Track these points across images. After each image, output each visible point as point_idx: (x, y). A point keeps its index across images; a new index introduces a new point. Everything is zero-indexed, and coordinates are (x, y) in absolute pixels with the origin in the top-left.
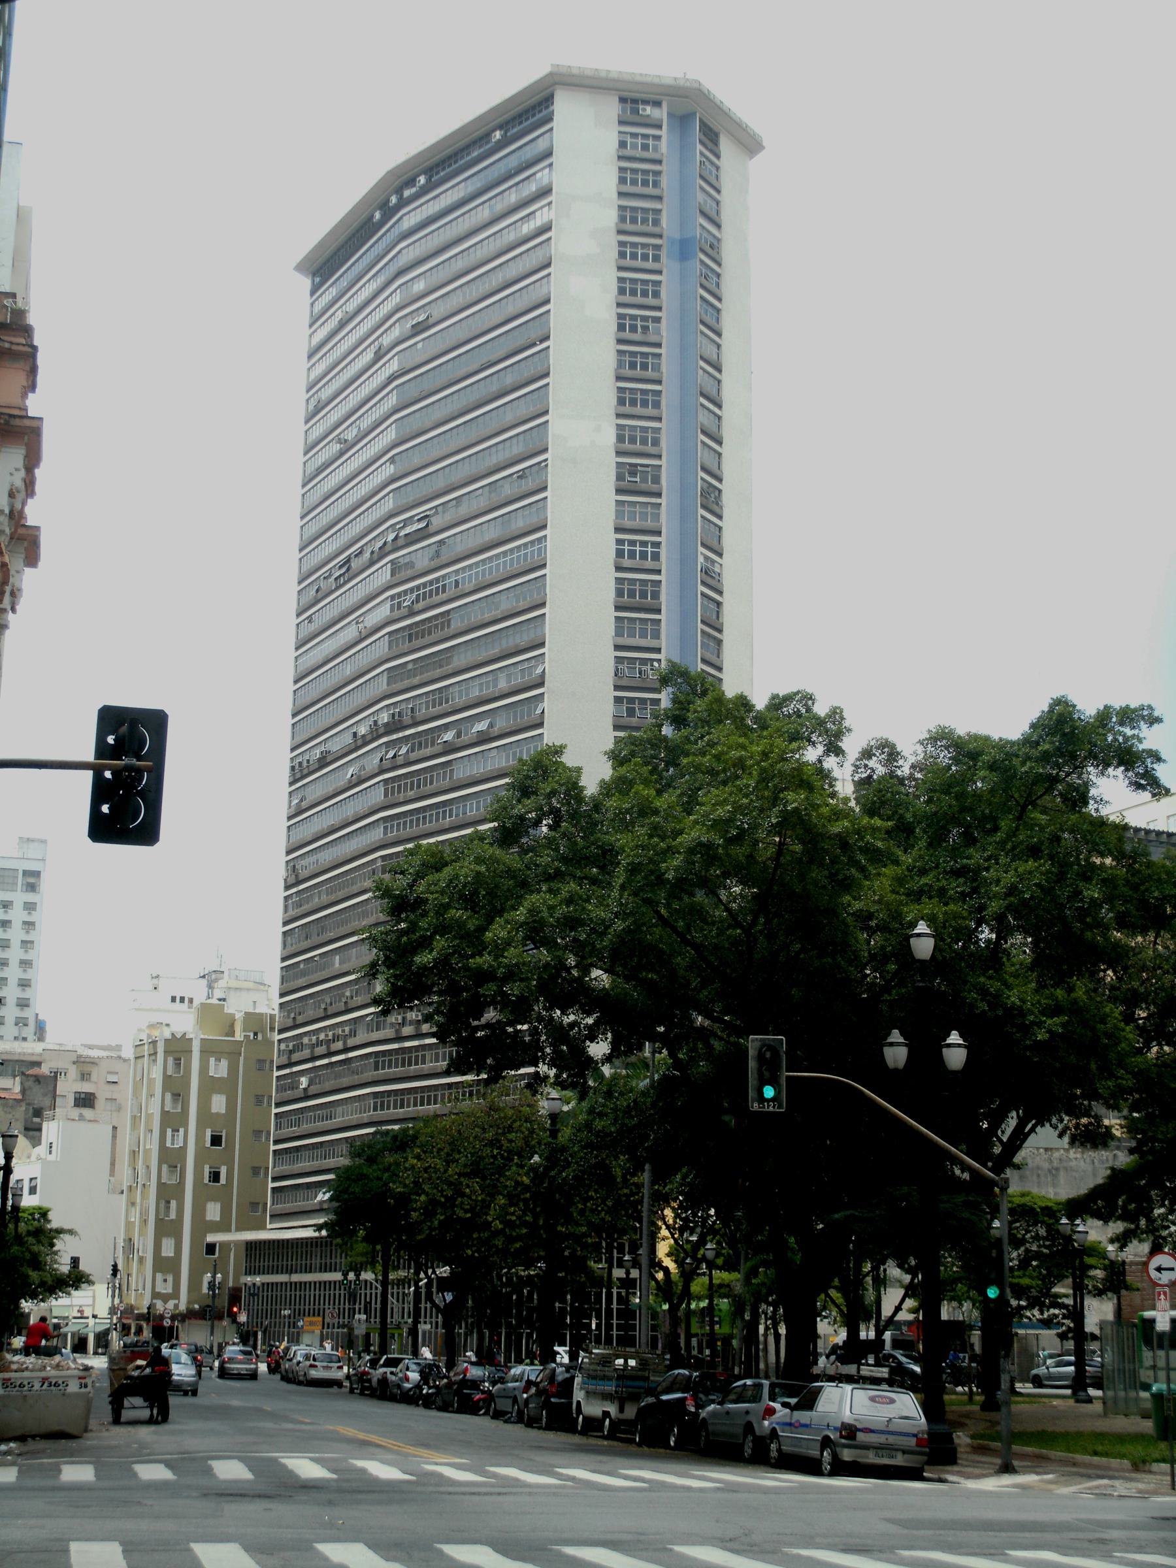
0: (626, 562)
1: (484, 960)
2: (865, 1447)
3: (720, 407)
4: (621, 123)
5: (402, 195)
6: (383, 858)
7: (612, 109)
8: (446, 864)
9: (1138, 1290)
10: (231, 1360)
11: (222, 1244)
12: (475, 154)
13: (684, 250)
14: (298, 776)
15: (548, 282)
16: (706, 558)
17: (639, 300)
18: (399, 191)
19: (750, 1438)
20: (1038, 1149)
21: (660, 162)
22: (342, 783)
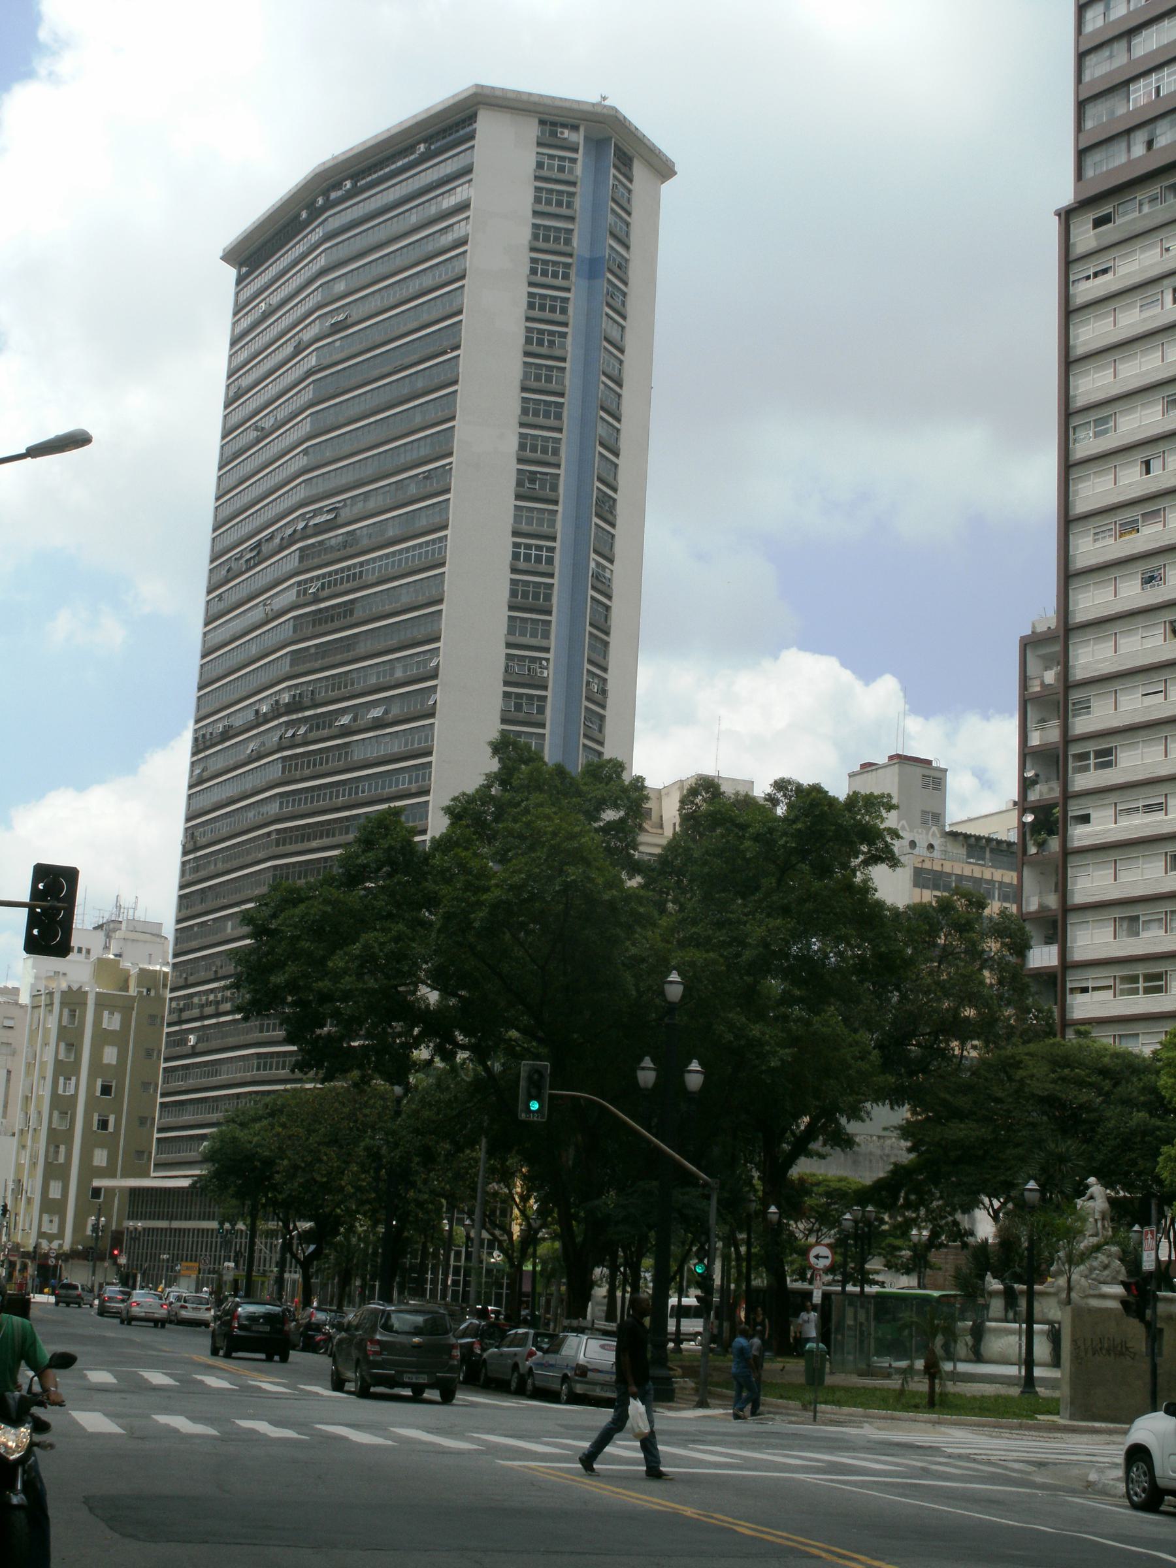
0: (522, 565)
1: (324, 985)
2: (594, 1383)
3: (619, 420)
4: (539, 144)
5: (328, 198)
6: (278, 831)
7: (532, 130)
8: (302, 901)
9: (940, 1269)
10: (111, 1299)
11: (107, 1189)
12: (400, 163)
13: (593, 268)
14: (201, 747)
15: (462, 294)
16: (598, 564)
17: (547, 315)
18: (326, 193)
19: (516, 1375)
20: (871, 1136)
21: (574, 184)
22: (242, 757)
